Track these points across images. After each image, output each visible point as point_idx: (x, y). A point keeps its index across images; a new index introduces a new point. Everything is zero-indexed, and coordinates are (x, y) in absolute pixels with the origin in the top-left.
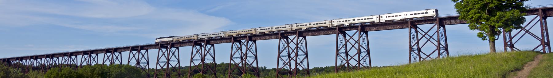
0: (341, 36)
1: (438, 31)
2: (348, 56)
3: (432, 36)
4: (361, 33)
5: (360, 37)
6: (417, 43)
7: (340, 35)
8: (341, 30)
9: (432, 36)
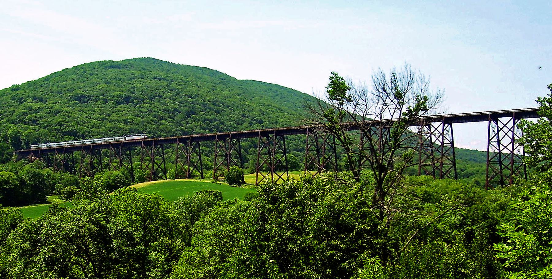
0: (493, 123)
2: (500, 145)
3: (506, 124)
7: (492, 122)
8: (493, 117)
9: (506, 124)
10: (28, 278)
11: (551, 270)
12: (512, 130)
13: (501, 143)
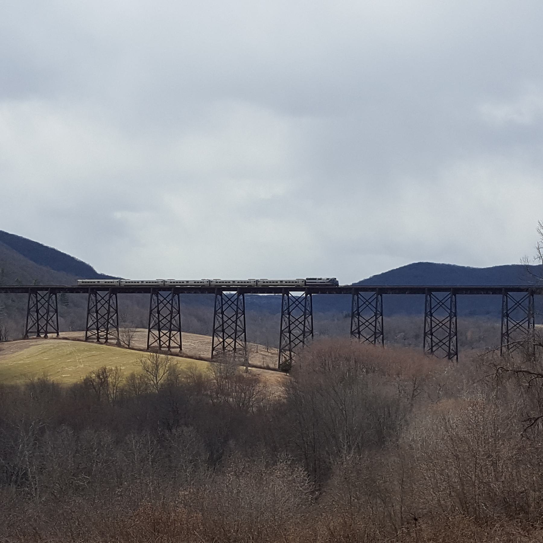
1: (377, 298)
4: (50, 295)
5: (49, 298)
6: (288, 308)
10: (251, 542)
11: (542, 490)
12: (171, 303)
13: (160, 313)
